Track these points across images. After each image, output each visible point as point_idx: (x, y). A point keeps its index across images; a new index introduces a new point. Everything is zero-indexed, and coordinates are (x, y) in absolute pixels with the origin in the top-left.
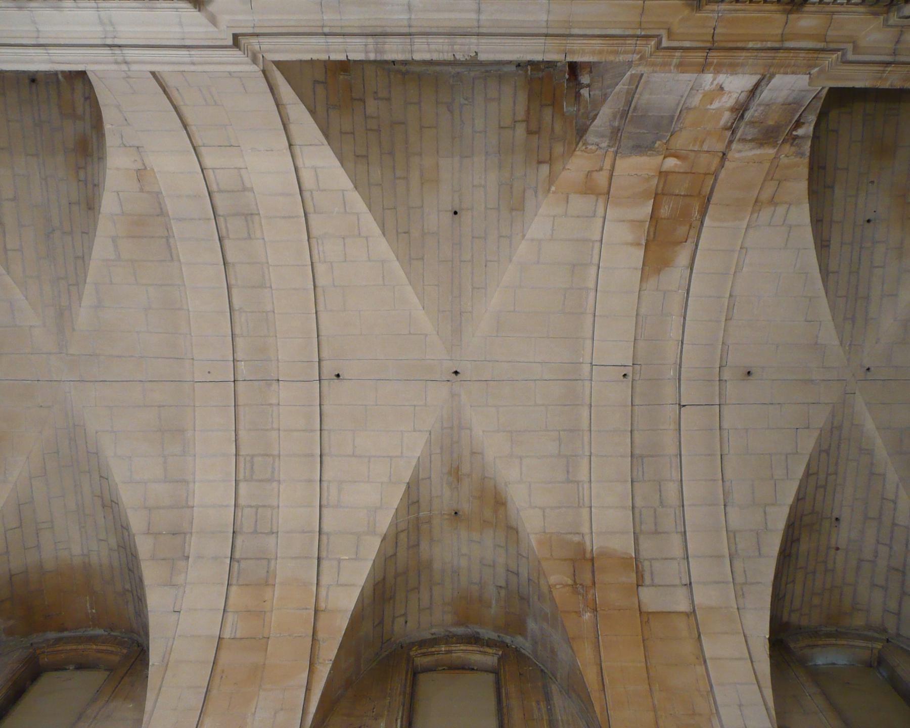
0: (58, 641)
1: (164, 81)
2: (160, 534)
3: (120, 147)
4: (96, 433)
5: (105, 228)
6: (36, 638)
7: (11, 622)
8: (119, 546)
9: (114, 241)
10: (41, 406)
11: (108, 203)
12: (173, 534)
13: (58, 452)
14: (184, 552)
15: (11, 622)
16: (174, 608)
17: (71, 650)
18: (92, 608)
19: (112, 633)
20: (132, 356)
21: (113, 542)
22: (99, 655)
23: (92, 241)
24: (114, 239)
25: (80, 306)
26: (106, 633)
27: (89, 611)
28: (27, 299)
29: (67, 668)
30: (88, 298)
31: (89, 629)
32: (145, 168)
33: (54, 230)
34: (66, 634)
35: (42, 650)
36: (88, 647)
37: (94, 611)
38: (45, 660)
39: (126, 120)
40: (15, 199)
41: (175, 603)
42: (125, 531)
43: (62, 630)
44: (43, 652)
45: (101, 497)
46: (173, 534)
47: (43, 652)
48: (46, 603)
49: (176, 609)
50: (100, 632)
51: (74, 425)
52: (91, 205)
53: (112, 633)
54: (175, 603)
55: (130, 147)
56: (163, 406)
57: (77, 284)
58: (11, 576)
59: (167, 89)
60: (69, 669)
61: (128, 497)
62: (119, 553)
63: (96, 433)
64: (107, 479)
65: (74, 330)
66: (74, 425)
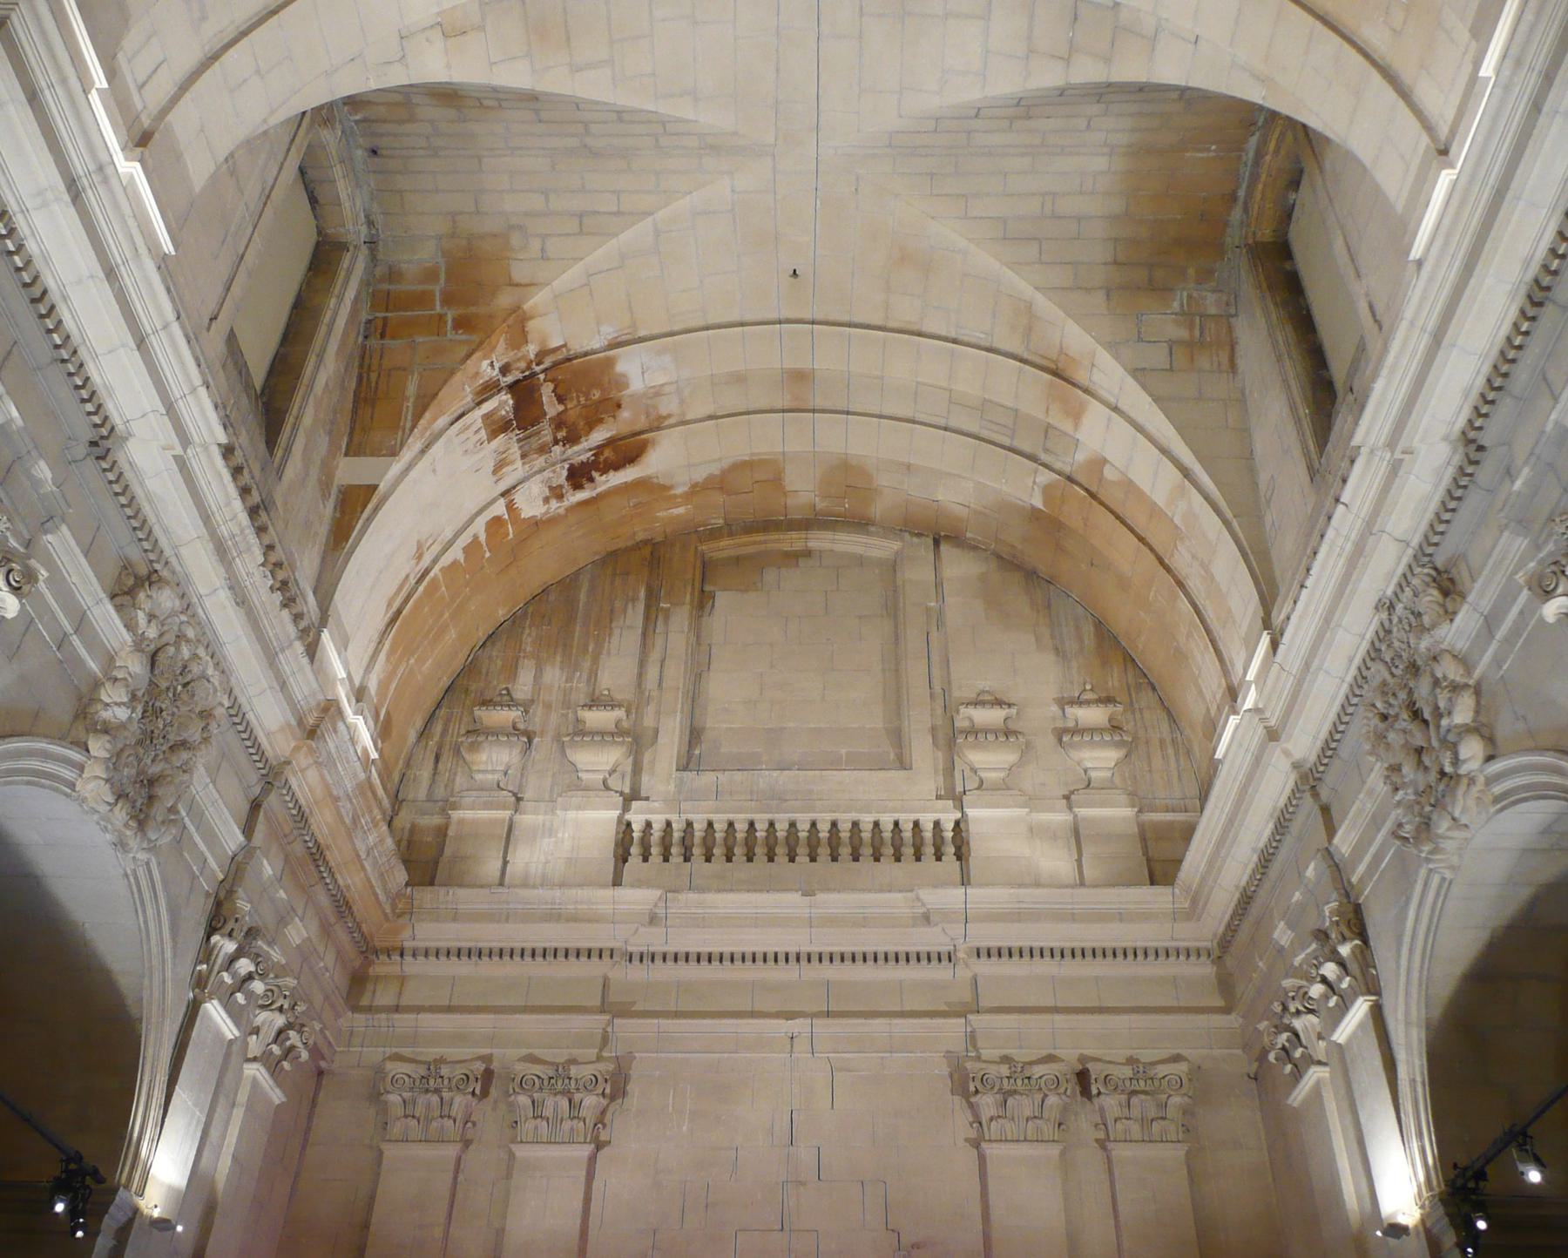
0: (1246, 210)
1: (251, 19)
2: (1071, 41)
3: (407, 66)
4: (901, 117)
5: (556, 81)
6: (1233, 237)
7: (1191, 272)
8: (1098, 102)
9: (579, 70)
10: (856, 190)
11: (514, 76)
12: (1076, 19)
13: (932, 175)
14: (1108, 7)
15: (1191, 272)
16: (1190, 42)
17: (1263, 193)
18: (1208, 150)
19: (1260, 124)
20: (777, 51)
21: (1093, 109)
22: (1283, 152)
23: (585, 101)
24: (576, 69)
25: (696, 121)
26: (1258, 134)
27: (1212, 154)
28: (690, 193)
29: (1292, 202)
30: (685, 110)
31: (1244, 159)
32: (439, 24)
33: (585, 146)
34: (1241, 193)
35: (1250, 234)
36: (1266, 166)
37: (1213, 147)
38: (1266, 233)
39: (353, 60)
40: (546, 193)
41: (1183, 39)
42: (1066, 93)
43: (1233, 198)
44: (1254, 233)
45: (1012, 119)
46: (1076, 19)
47: (1254, 233)
48: (1179, 217)
49: (1193, 39)
50: (1253, 141)
51: (890, 146)
52: (531, 98)
53: (1260, 124)
54: (1183, 39)
55: (403, 50)
56: (861, 7)
57: (664, 124)
58: (1115, 263)
59: (271, 8)
60: (1295, 200)
61: (1007, 83)
62: (1113, 102)
63: (901, 117)
64: (979, 109)
65: (735, 133)
66: (890, 146)
